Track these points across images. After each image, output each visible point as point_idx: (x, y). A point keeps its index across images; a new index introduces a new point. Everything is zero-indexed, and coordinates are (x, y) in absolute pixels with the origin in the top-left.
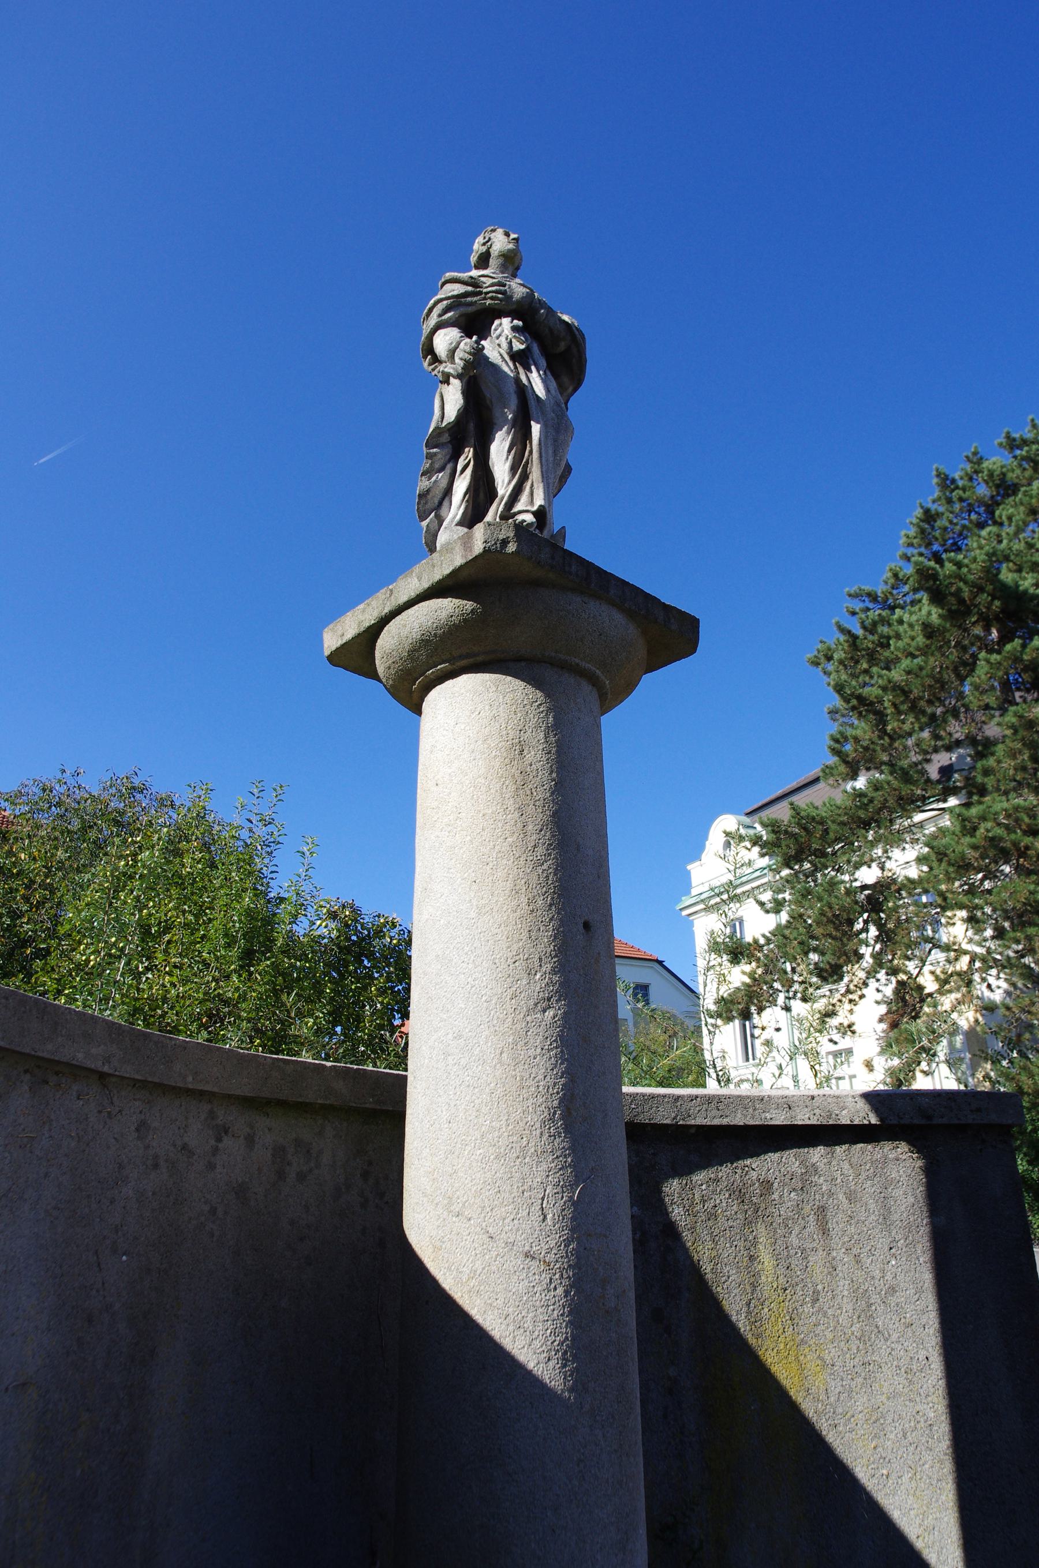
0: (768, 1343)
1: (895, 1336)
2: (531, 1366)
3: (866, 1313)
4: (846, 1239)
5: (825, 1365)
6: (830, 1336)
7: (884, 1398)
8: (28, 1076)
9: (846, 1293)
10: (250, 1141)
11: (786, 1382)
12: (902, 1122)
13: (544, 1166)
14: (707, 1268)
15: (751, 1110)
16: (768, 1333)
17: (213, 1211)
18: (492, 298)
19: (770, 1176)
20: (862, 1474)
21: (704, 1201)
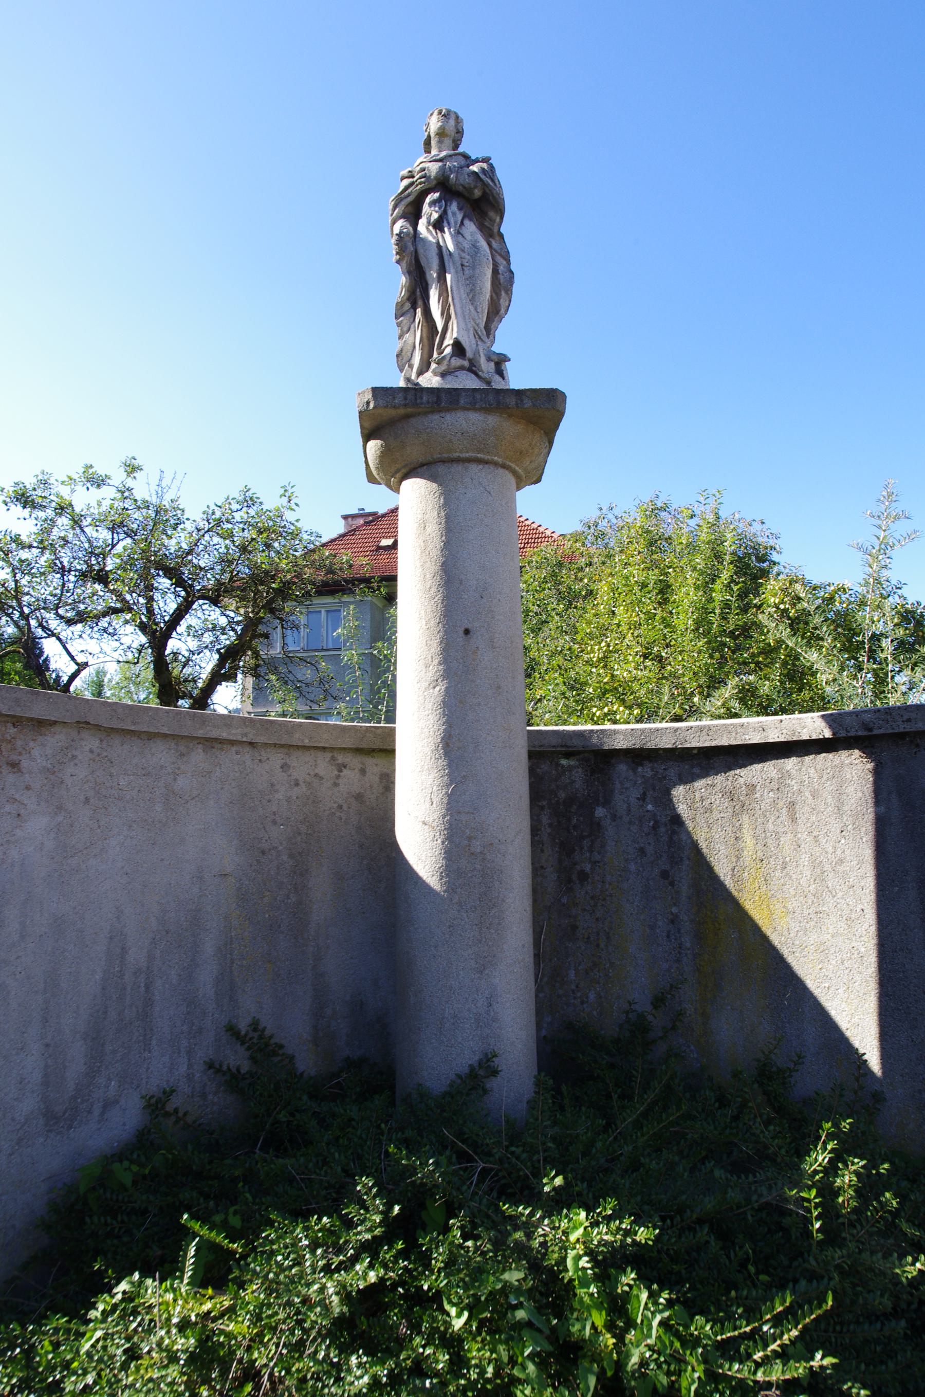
0: (746, 895)
1: (840, 895)
2: (424, 878)
3: (820, 877)
4: (809, 825)
5: (788, 912)
6: (793, 892)
7: (829, 936)
8: (201, 746)
9: (806, 863)
10: (363, 772)
11: (760, 923)
12: (849, 735)
13: (432, 776)
14: (703, 845)
15: (734, 734)
16: (747, 889)
17: (340, 807)
18: (420, 183)
19: (754, 781)
20: (811, 984)
21: (702, 800)
